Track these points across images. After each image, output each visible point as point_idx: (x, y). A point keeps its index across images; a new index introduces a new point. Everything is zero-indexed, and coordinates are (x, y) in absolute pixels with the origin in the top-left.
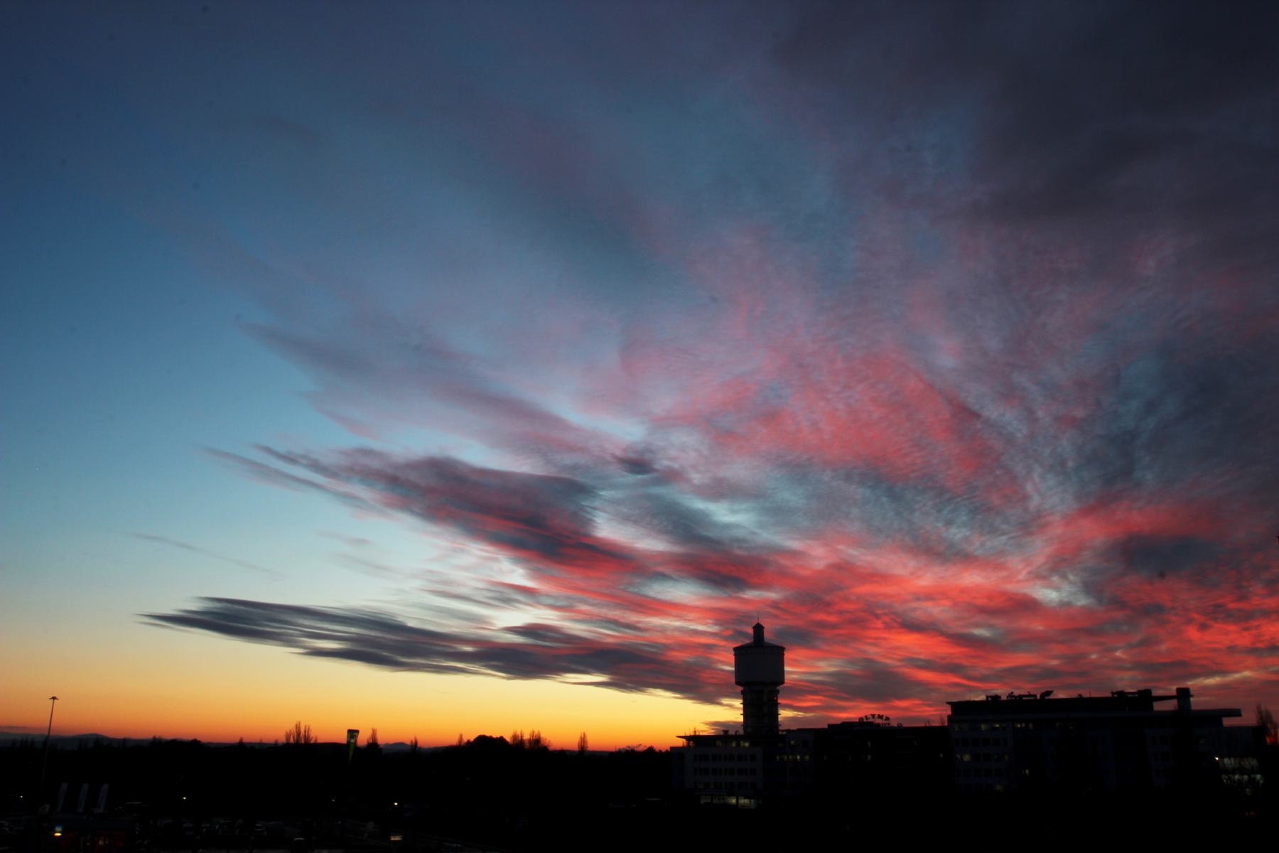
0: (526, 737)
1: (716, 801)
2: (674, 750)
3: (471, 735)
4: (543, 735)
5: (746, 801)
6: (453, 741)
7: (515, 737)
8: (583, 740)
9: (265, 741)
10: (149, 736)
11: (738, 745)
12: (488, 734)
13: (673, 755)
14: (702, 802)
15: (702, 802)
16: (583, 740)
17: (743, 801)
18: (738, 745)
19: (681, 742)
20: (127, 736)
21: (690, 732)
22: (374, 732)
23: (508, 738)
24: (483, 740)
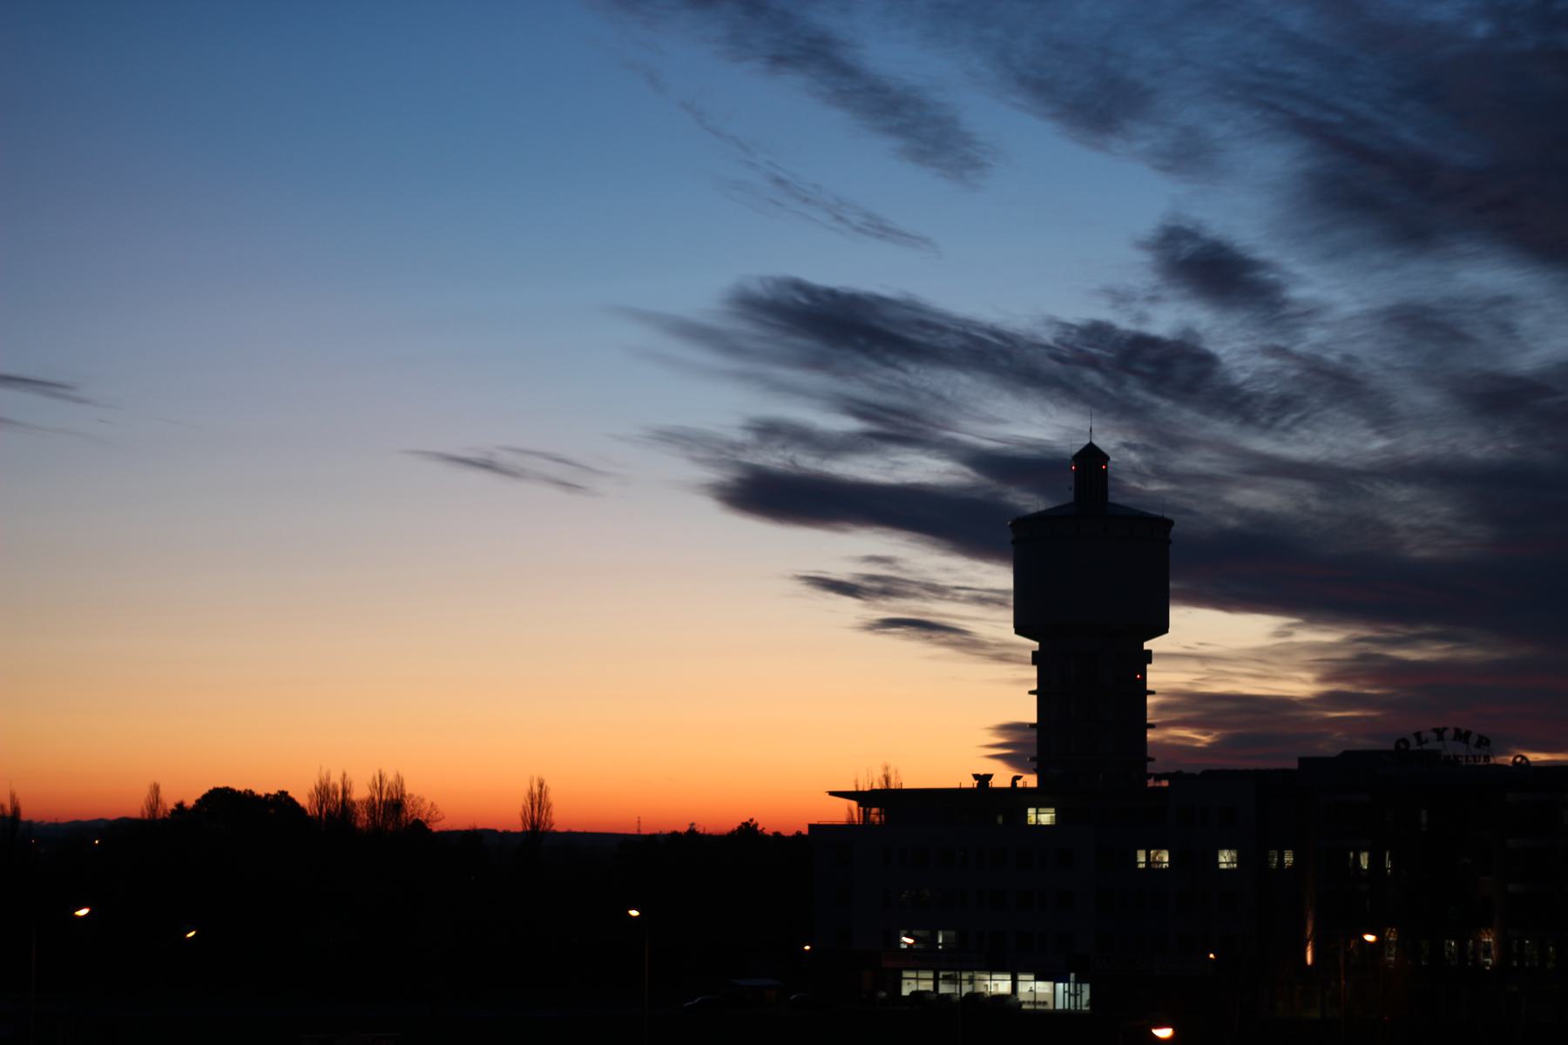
0: (361, 792)
1: (944, 989)
2: (821, 832)
3: (186, 787)
4: (408, 790)
5: (1043, 988)
6: (133, 804)
7: (324, 792)
8: (538, 800)
9: (61, 821)
10: (69, 819)
11: (1193, 859)
12: (231, 786)
13: (475, 846)
14: (906, 991)
15: (906, 991)
16: (538, 800)
17: (1034, 989)
18: (1193, 859)
19: (842, 812)
20: (481, 824)
21: (870, 780)
22: (156, 789)
23: (302, 795)
24: (222, 802)
